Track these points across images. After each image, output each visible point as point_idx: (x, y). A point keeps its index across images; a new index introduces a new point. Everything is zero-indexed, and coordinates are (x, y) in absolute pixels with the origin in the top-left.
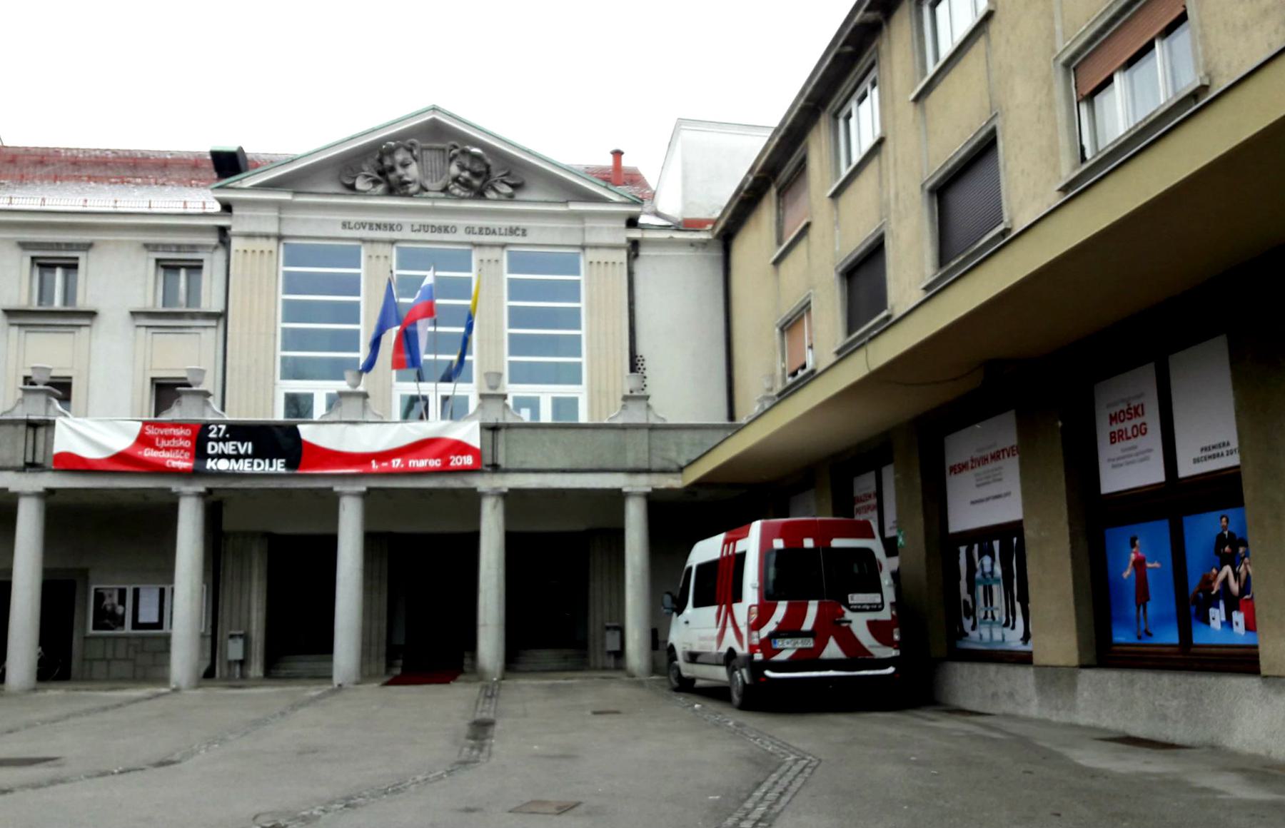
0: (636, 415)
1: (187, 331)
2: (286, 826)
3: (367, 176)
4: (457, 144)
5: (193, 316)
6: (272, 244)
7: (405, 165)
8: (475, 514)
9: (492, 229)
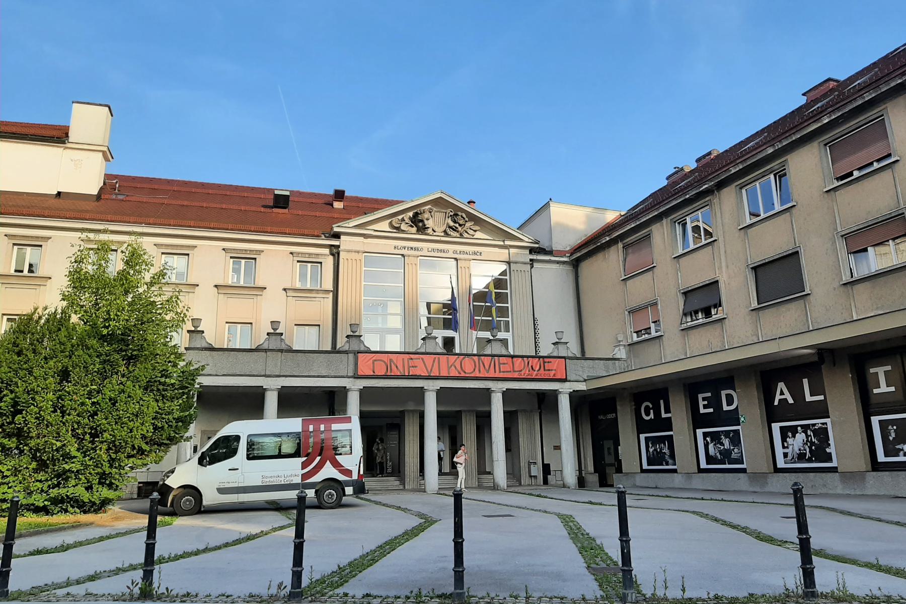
0: (274, 344)
1: (314, 299)
2: (393, 602)
3: (407, 223)
4: (452, 211)
5: (317, 291)
6: (400, 256)
7: (428, 219)
8: (489, 402)
9: (466, 252)
